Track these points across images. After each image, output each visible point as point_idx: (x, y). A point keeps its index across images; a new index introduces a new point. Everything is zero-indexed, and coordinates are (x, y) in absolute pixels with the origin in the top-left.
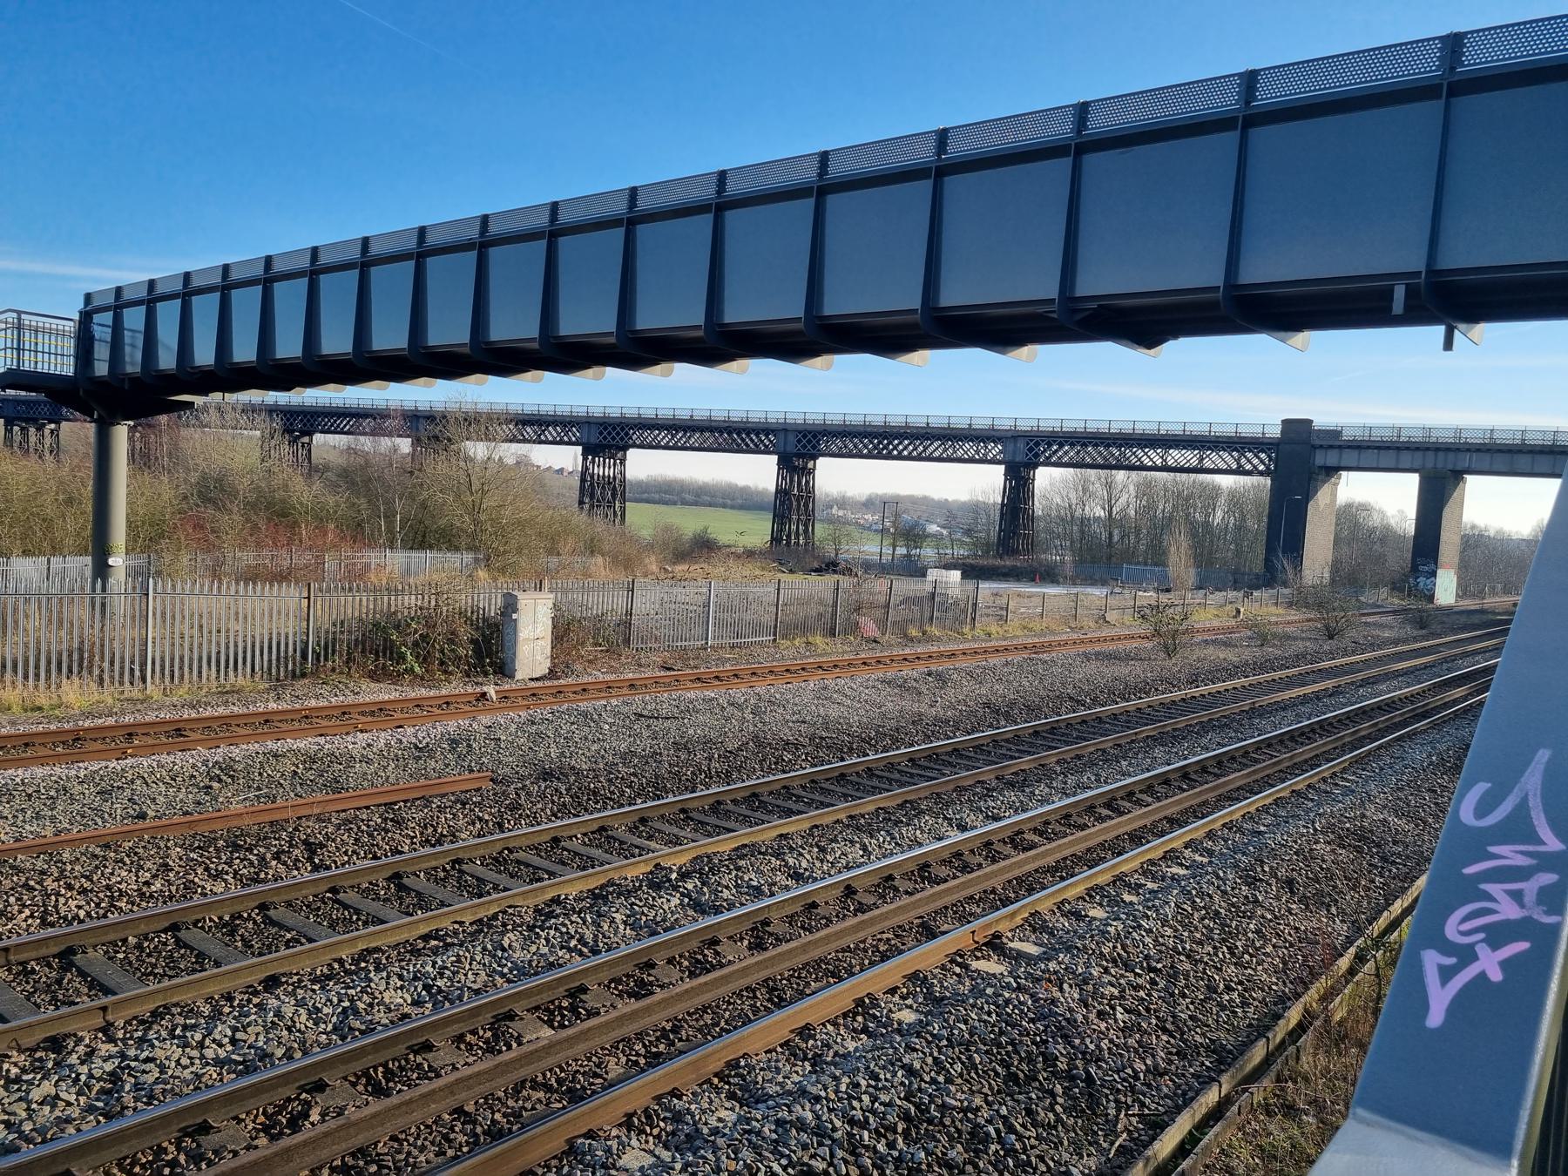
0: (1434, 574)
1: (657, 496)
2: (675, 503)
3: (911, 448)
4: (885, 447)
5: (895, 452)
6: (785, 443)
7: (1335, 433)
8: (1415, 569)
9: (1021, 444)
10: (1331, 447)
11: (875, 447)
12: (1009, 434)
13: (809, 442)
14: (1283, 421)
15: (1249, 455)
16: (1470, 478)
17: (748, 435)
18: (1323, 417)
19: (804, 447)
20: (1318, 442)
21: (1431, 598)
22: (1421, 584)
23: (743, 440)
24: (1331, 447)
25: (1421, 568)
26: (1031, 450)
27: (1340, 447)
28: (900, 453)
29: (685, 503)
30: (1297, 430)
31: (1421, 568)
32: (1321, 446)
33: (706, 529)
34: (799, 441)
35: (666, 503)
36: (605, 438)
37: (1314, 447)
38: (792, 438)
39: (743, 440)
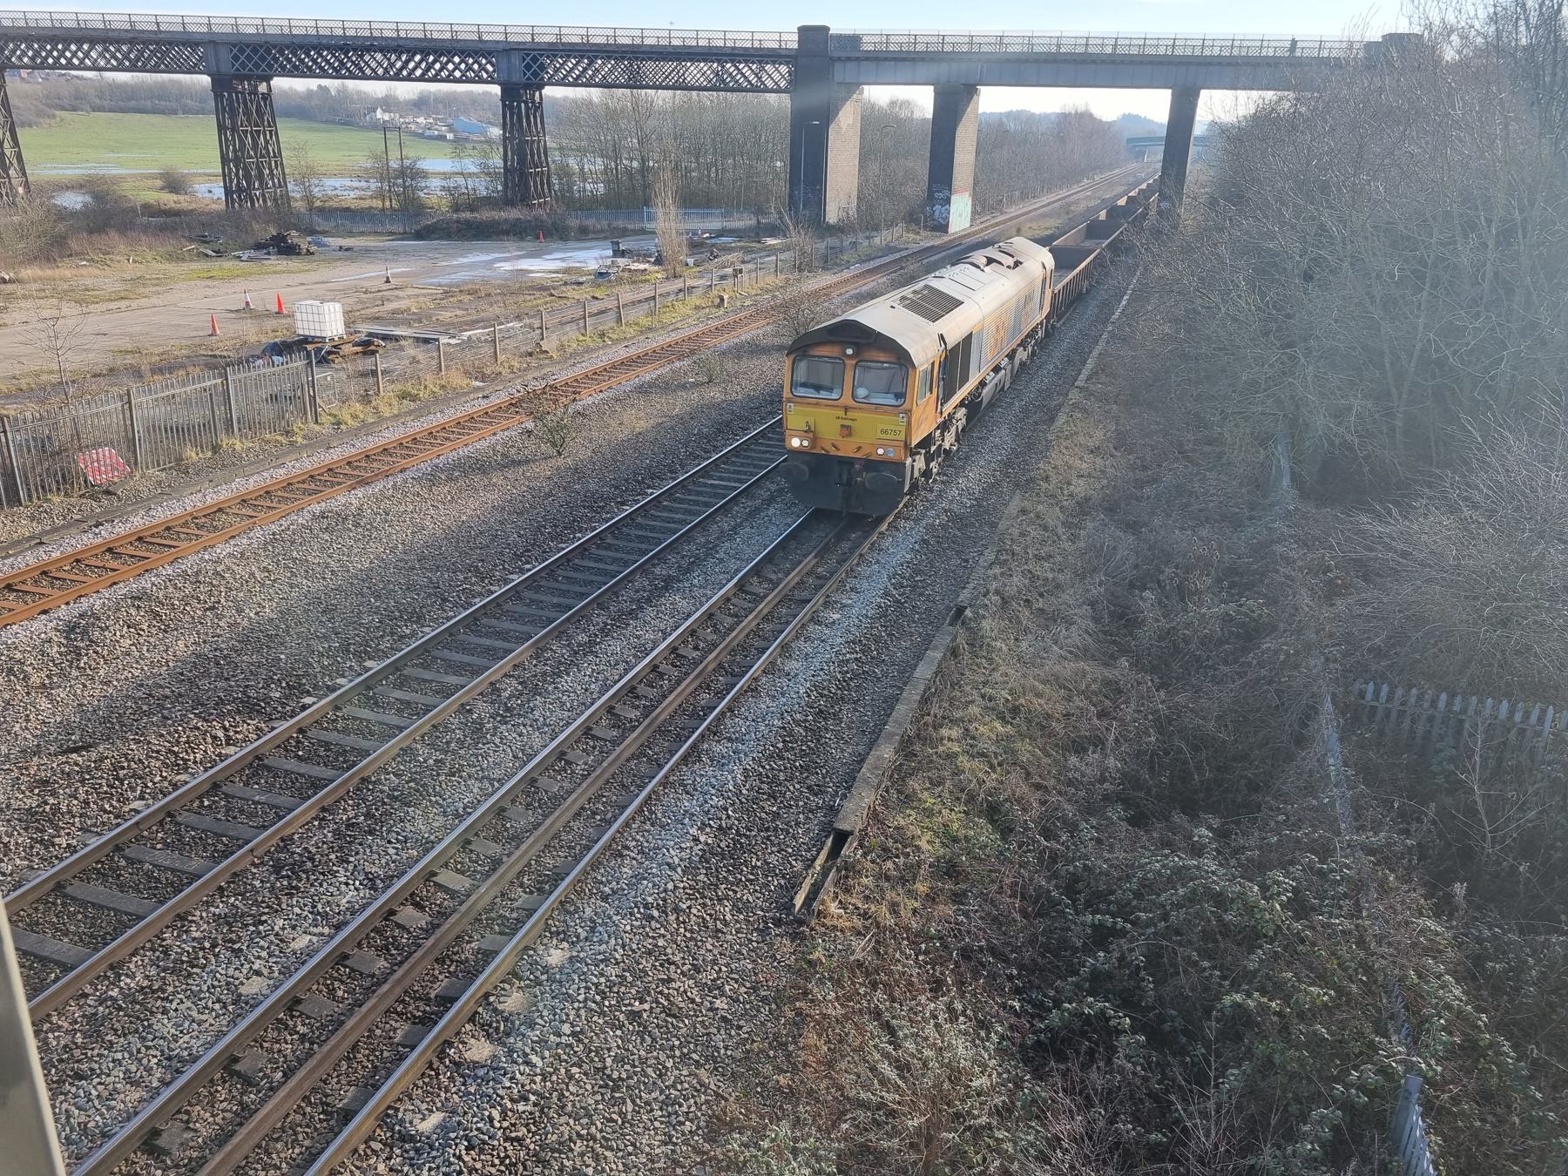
0: (948, 201)
1: (149, 103)
2: (174, 112)
3: (437, 66)
4: (74, 54)
5: (50, 61)
6: (217, 61)
7: (854, 40)
8: (931, 198)
9: (516, 60)
10: (849, 59)
11: (126, 57)
12: (501, 47)
13: (263, 59)
14: (799, 29)
15: (367, 58)
16: (983, 90)
17: (281, 52)
18: (839, 25)
19: (243, 65)
20: (836, 55)
21: (943, 228)
22: (937, 213)
23: (315, 61)
24: (849, 59)
25: (936, 195)
26: (528, 67)
27: (857, 59)
28: (69, 61)
29: (187, 111)
30: (813, 36)
31: (936, 195)
32: (839, 59)
34: (236, 58)
35: (162, 112)
36: (243, 65)
37: (833, 60)
38: (225, 55)
39: (315, 61)
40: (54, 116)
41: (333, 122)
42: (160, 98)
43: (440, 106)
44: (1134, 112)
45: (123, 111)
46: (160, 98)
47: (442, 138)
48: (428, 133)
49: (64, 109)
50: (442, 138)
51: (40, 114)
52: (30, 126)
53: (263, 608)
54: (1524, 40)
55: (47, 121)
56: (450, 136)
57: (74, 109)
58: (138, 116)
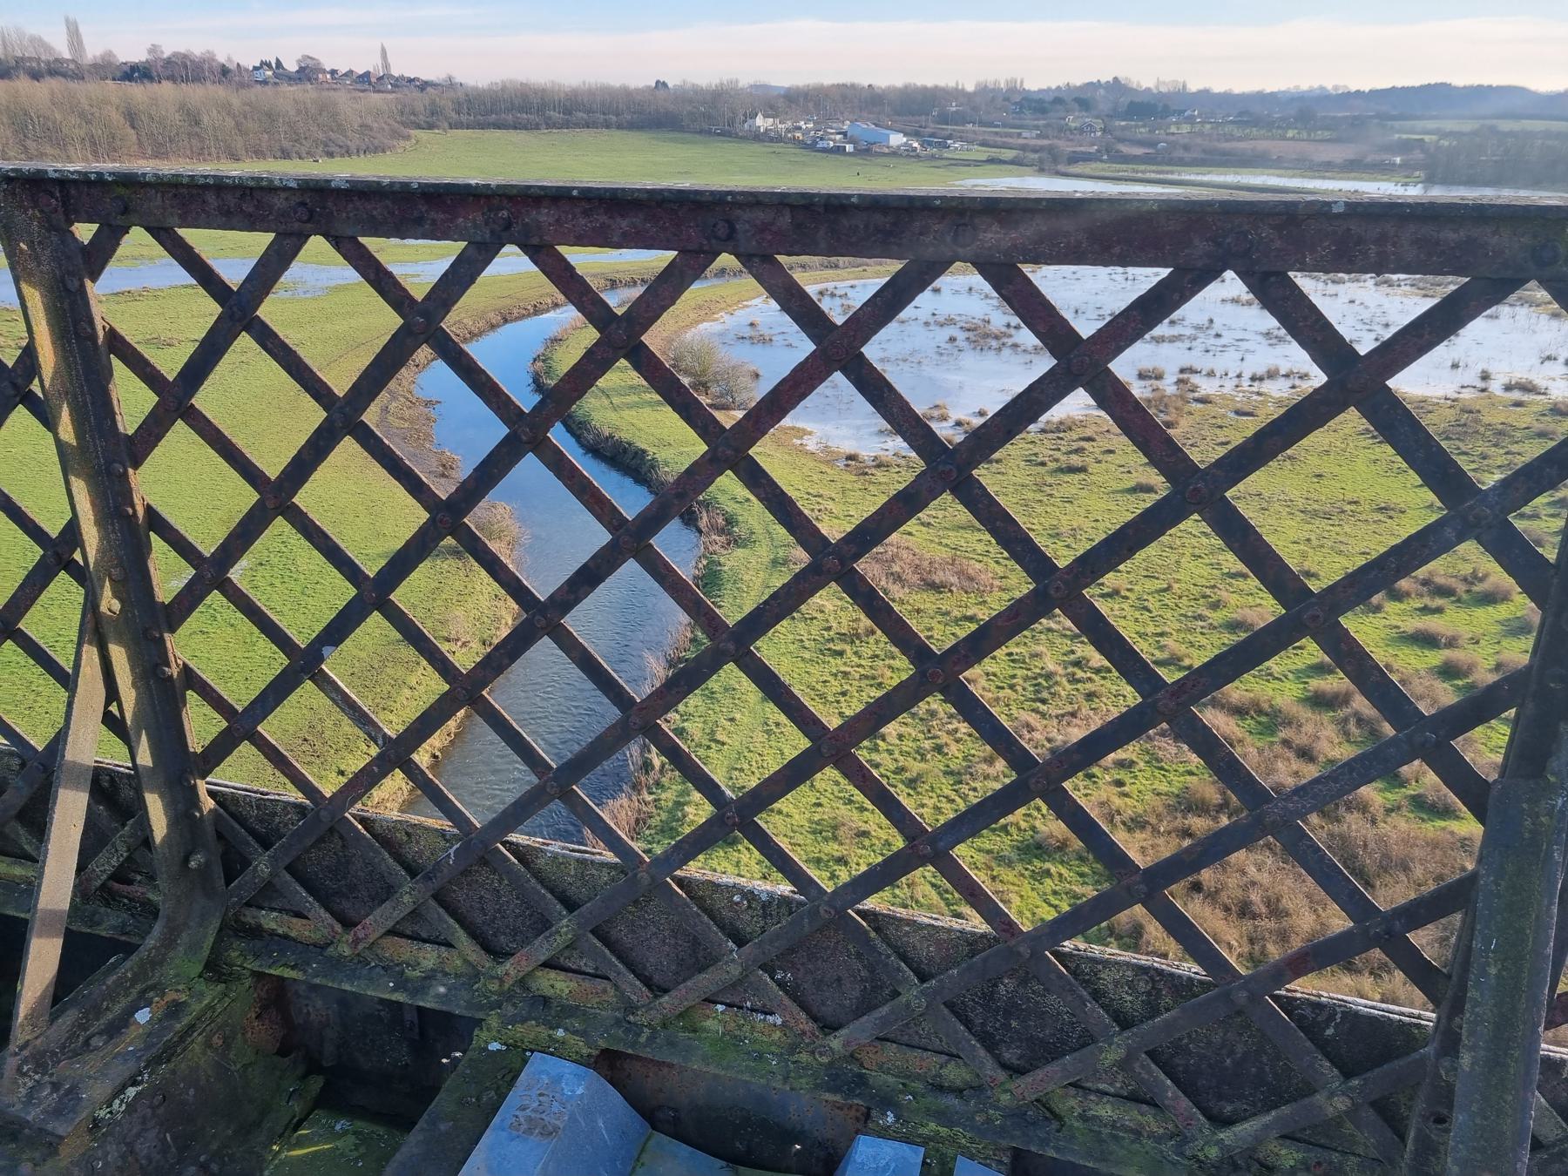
2: (537, 127)
29: (551, 125)
33: (737, 81)
35: (516, 126)
40: (408, 138)
41: (709, 133)
42: (522, 109)
43: (811, 105)
44: (176, 50)
45: (482, 126)
46: (522, 109)
47: (839, 150)
48: (821, 144)
49: (419, 127)
50: (839, 150)
51: (396, 135)
52: (384, 151)
53: (22, 804)
54: (942, 844)
55: (402, 143)
56: (849, 148)
57: (431, 126)
58: (498, 133)
